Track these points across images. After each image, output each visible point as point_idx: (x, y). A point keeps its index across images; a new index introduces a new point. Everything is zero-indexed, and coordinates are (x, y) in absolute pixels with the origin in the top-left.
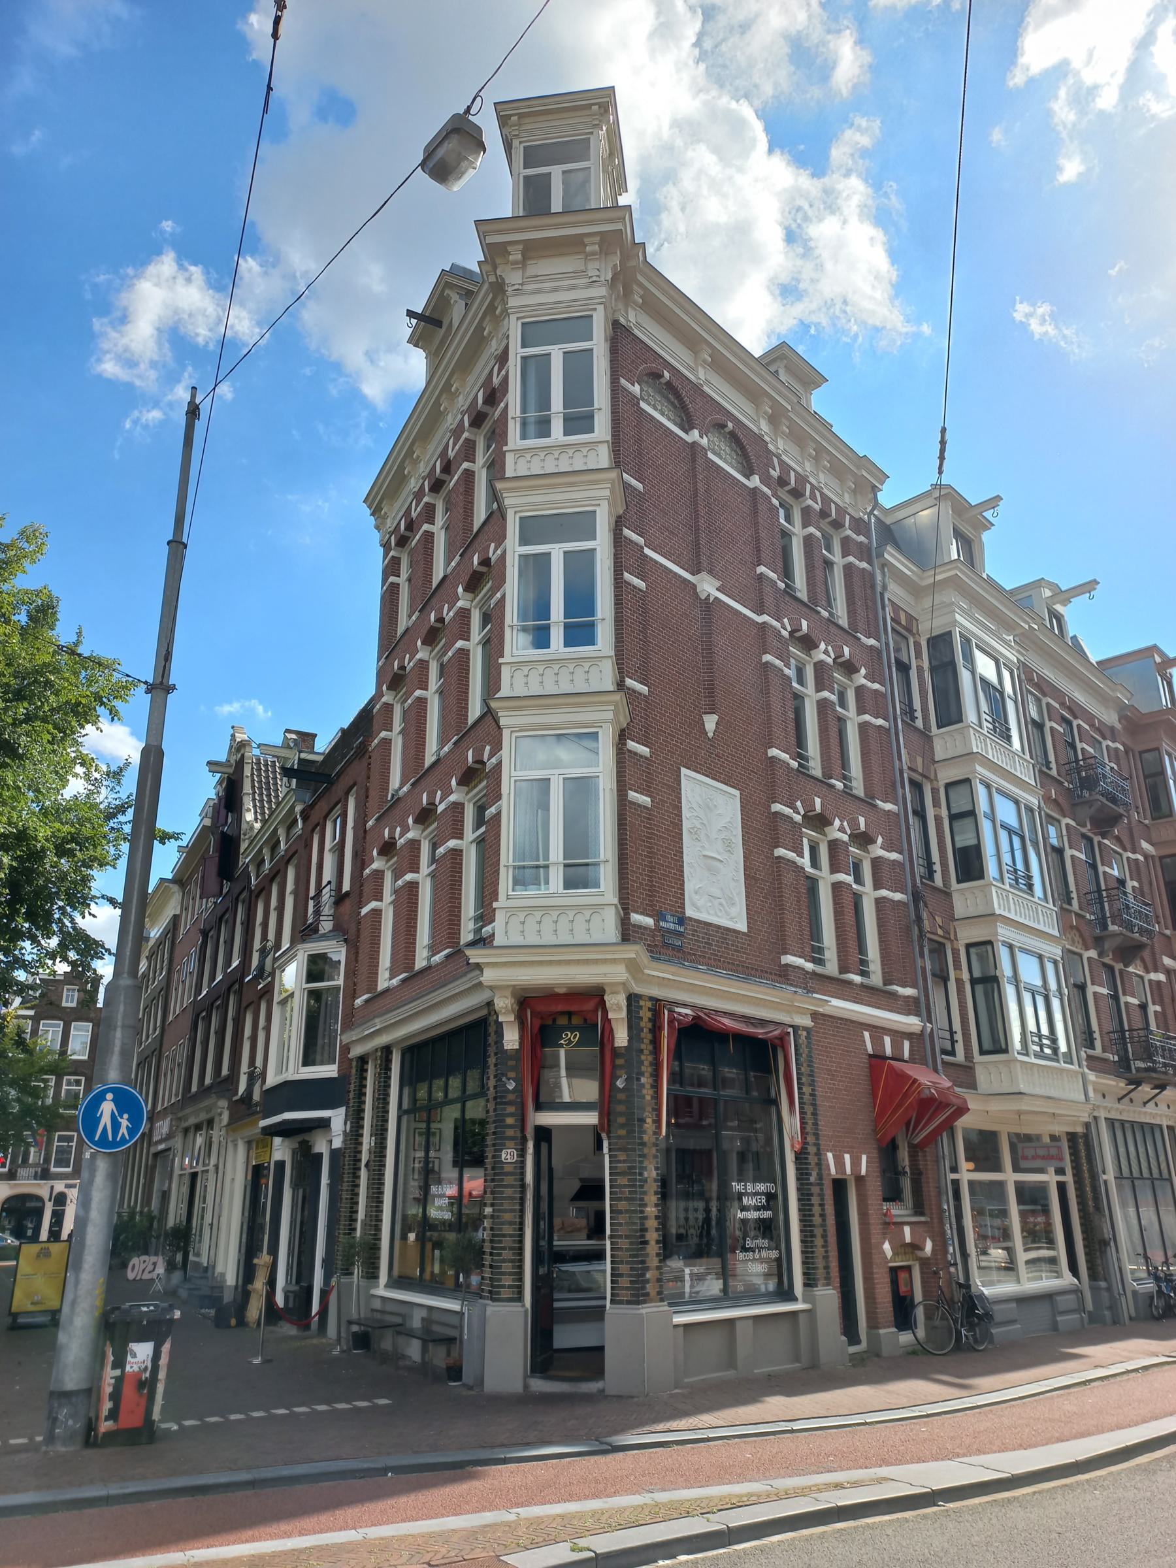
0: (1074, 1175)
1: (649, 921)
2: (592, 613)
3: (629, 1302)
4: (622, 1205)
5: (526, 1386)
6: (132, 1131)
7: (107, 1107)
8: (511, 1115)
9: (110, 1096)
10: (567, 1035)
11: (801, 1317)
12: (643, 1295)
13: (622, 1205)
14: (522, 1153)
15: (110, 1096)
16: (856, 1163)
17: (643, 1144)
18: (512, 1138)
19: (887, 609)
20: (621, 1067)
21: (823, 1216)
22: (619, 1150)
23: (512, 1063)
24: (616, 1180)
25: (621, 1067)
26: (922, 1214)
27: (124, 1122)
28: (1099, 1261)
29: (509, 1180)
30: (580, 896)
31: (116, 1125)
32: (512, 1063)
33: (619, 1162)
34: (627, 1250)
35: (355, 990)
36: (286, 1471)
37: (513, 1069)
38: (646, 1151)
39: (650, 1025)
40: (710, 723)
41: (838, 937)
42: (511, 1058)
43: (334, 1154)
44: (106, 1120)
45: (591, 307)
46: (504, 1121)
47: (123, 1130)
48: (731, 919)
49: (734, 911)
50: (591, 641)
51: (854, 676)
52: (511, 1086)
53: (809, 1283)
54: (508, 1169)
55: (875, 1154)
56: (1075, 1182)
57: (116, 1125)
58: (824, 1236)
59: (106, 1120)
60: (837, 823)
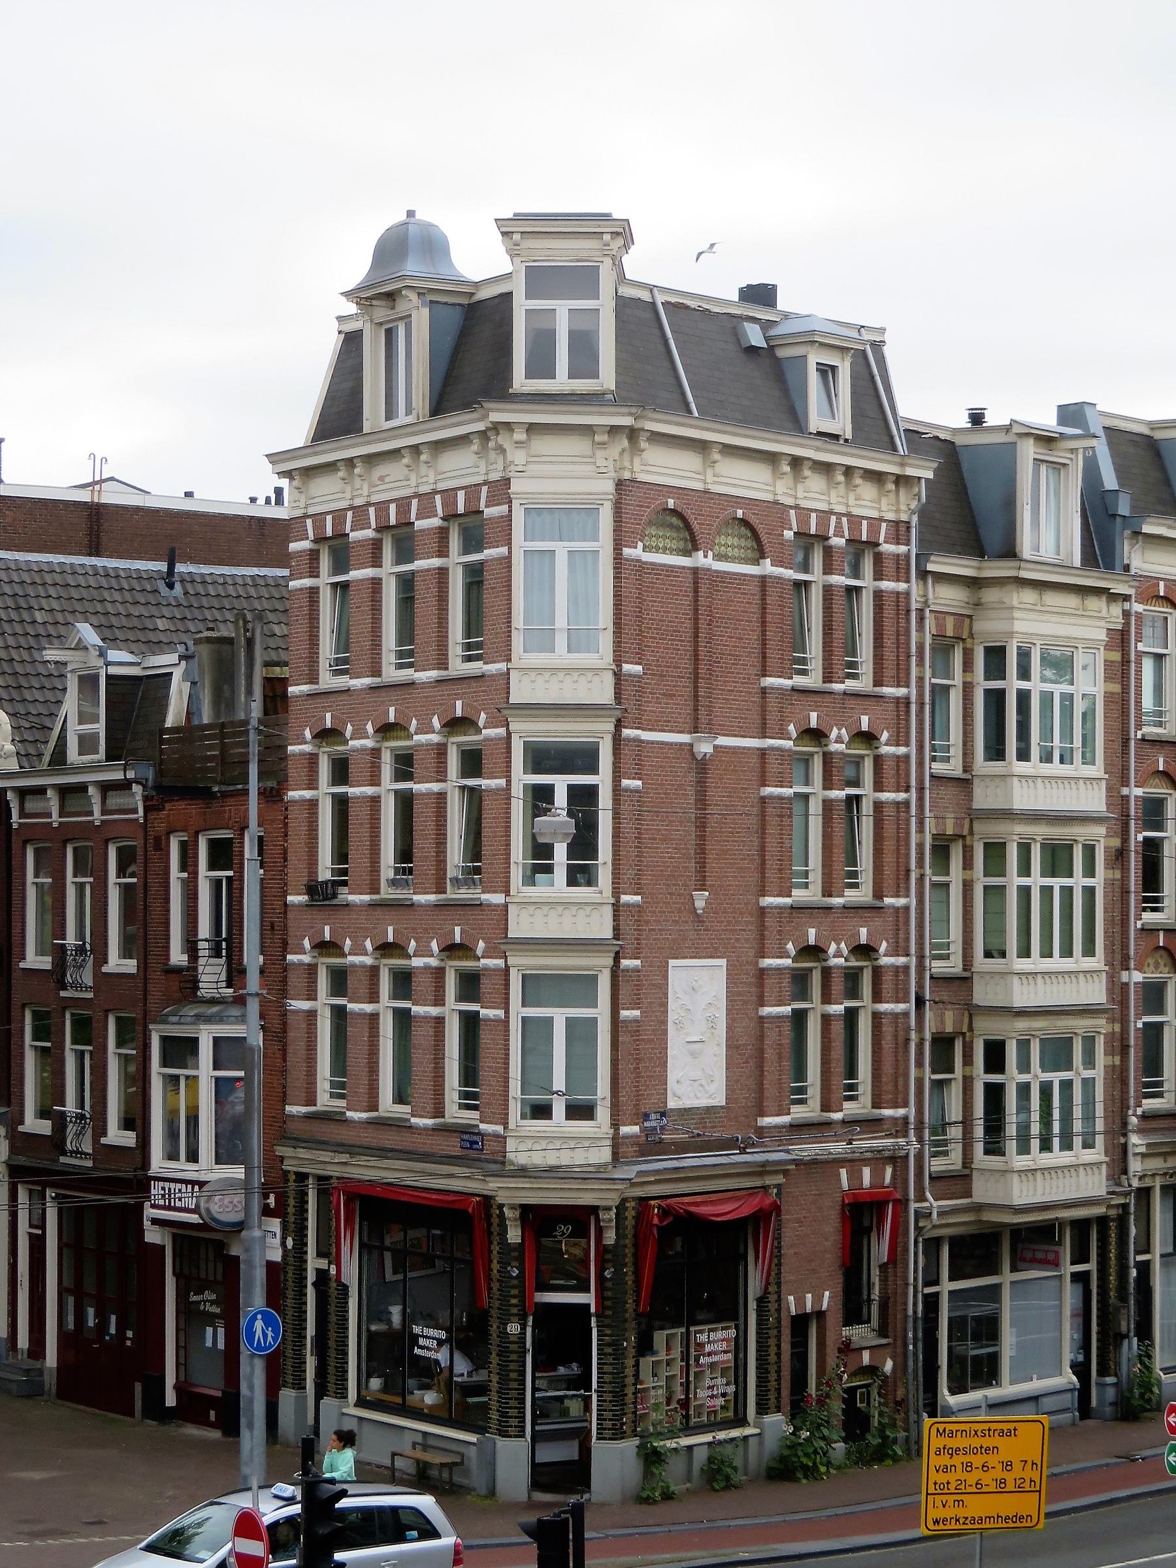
0: (1098, 1263)
1: (635, 1129)
2: (595, 857)
3: (610, 1439)
4: (607, 1368)
5: (529, 1497)
6: (275, 1339)
7: (259, 1324)
8: (514, 1297)
9: (259, 1316)
10: (560, 1228)
11: (752, 1441)
12: (622, 1433)
13: (607, 1368)
14: (524, 1328)
15: (259, 1316)
16: (818, 1299)
17: (626, 1321)
18: (516, 1315)
19: (927, 622)
20: (608, 1261)
21: (778, 1355)
22: (606, 1326)
23: (515, 1254)
24: (602, 1350)
25: (608, 1261)
26: (886, 1337)
27: (270, 1334)
28: (1112, 1356)
29: (513, 1347)
30: (581, 1127)
31: (265, 1336)
32: (515, 1254)
33: (606, 1335)
34: (610, 1401)
35: (284, 1093)
36: (488, 1541)
37: (516, 1259)
38: (627, 1325)
39: (633, 1231)
40: (701, 900)
41: (823, 1073)
42: (515, 1250)
43: (271, 1266)
44: (259, 1333)
45: (598, 502)
46: (509, 1301)
47: (270, 1338)
48: (710, 1097)
49: (712, 1088)
50: (591, 882)
51: (875, 743)
52: (515, 1272)
53: (762, 1409)
54: (512, 1339)
55: (839, 1288)
56: (1098, 1271)
57: (265, 1336)
58: (778, 1372)
59: (259, 1333)
60: (833, 947)
